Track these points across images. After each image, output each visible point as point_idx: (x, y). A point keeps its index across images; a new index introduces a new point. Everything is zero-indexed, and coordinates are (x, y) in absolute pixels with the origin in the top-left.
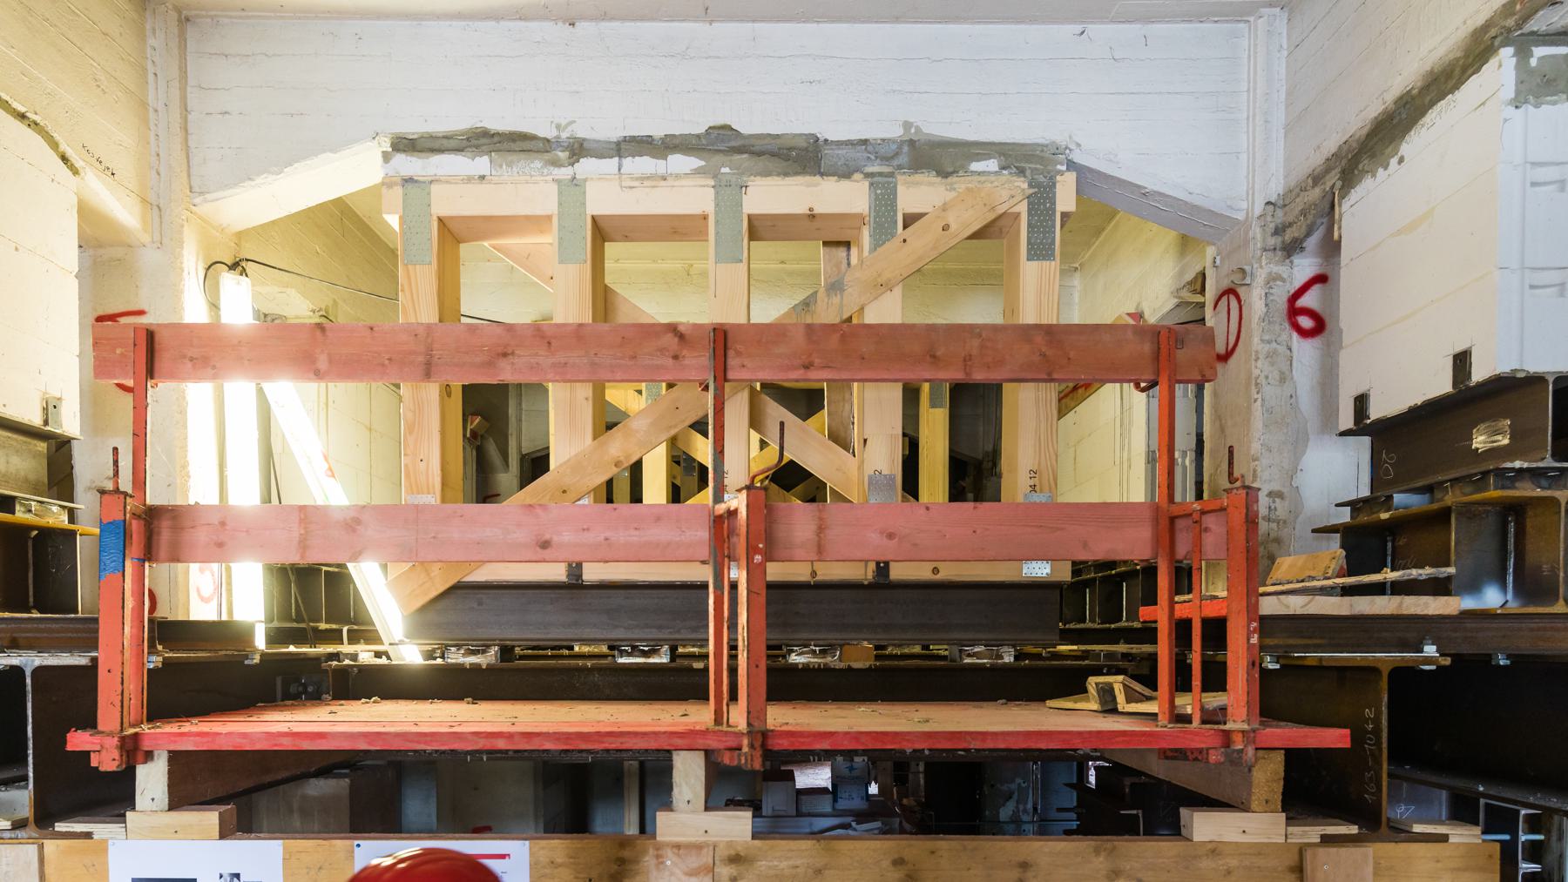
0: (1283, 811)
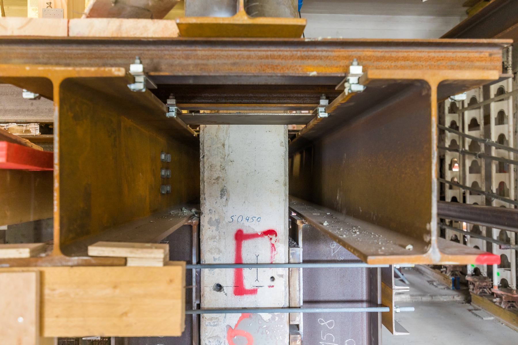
0: (400, 311)
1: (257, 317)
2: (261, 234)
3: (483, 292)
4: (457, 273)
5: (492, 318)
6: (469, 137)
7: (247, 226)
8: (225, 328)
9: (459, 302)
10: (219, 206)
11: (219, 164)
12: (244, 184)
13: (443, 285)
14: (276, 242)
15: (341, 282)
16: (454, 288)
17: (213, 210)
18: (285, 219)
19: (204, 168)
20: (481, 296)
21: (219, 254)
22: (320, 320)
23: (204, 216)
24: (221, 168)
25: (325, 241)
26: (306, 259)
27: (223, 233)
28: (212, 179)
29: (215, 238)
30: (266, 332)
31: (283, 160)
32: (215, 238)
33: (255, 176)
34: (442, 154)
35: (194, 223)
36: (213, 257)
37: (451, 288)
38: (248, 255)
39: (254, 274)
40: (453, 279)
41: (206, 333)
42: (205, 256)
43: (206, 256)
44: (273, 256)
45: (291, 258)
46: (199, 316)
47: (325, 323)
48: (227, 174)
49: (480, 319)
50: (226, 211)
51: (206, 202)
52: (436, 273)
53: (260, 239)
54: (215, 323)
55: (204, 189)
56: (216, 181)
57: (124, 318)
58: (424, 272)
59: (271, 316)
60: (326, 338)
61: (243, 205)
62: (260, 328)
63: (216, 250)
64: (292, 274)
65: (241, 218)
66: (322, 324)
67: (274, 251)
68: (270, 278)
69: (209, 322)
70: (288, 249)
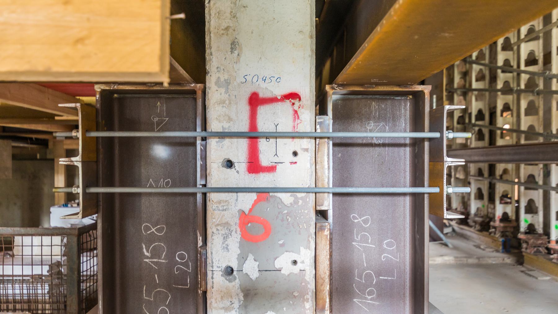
0: (453, 192)
1: (275, 200)
2: (281, 97)
3: (538, 251)
4: (507, 233)
5: (548, 278)
6: (525, 72)
7: (263, 89)
8: (236, 214)
9: (510, 265)
10: (229, 63)
11: (229, 10)
12: (260, 36)
13: (491, 248)
14: (299, 108)
15: (380, 171)
16: (504, 250)
17: (221, 67)
18: (310, 79)
19: (210, 15)
20: (536, 255)
21: (229, 123)
22: (354, 216)
23: (211, 76)
24: (231, 15)
25: (361, 120)
26: (336, 142)
27: (234, 97)
28: (220, 29)
29: (224, 102)
30: (287, 219)
31: (309, 6)
32: (224, 102)
33: (273, 26)
34: (492, 106)
35: (198, 87)
36: (221, 126)
37: (501, 251)
38: (264, 123)
39: (272, 147)
40: (503, 240)
41: (214, 219)
42: (212, 125)
43: (213, 125)
44: (296, 125)
45: (318, 129)
46: (205, 194)
47: (359, 220)
48: (238, 23)
49: (534, 279)
50: (238, 70)
51: (213, 58)
52: (483, 236)
53: (280, 105)
54: (225, 206)
55: (210, 42)
56: (225, 32)
57: (79, 46)
58: (469, 236)
59: (293, 199)
60: (360, 238)
61: (258, 62)
62: (279, 213)
63: (225, 117)
64: (320, 149)
65: (256, 78)
66: (356, 221)
67: (296, 119)
68: (295, 259)
69: (217, 205)
70: (315, 119)
